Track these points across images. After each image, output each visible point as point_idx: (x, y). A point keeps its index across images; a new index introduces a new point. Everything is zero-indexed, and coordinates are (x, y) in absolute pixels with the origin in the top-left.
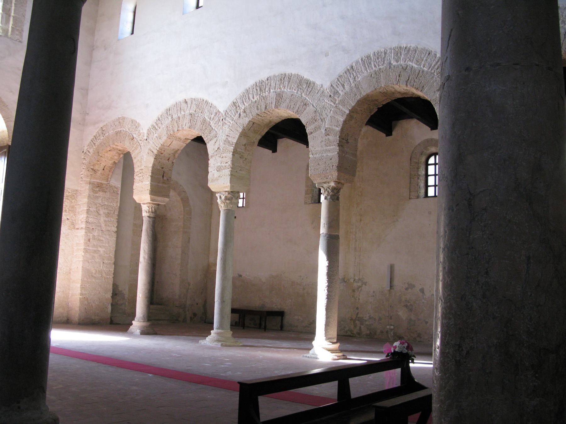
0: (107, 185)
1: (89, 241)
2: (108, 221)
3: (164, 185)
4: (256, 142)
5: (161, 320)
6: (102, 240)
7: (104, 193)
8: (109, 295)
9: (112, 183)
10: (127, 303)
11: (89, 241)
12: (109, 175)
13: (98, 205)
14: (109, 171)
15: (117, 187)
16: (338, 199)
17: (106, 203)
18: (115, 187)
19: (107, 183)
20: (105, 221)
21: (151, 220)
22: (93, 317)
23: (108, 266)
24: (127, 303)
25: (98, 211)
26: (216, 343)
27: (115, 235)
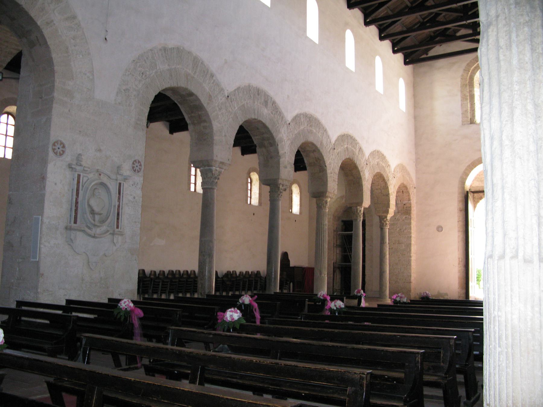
21: (385, 242)
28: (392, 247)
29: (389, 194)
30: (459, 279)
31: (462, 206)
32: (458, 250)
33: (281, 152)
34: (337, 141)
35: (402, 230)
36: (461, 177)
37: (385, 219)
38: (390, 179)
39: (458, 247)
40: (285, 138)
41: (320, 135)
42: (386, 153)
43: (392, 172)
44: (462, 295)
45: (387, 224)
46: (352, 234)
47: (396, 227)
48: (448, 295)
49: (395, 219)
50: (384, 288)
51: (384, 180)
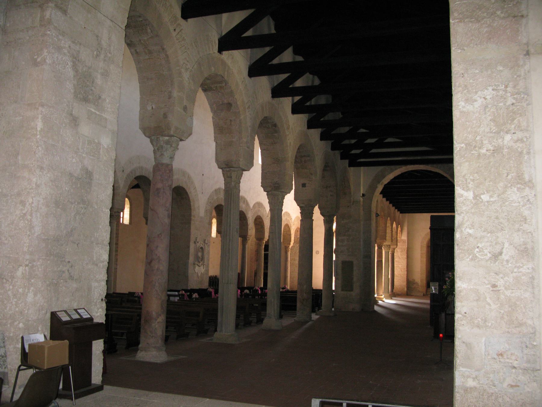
8: (405, 284)
10: (420, 287)
16: (255, 273)
17: (400, 247)
18: (404, 240)
26: (292, 144)
29: (291, 234)
33: (249, 223)
34: (185, 109)
35: (296, 253)
37: (288, 248)
38: (292, 226)
40: (250, 216)
41: (262, 211)
42: (290, 213)
43: (293, 222)
46: (268, 253)
51: (289, 227)
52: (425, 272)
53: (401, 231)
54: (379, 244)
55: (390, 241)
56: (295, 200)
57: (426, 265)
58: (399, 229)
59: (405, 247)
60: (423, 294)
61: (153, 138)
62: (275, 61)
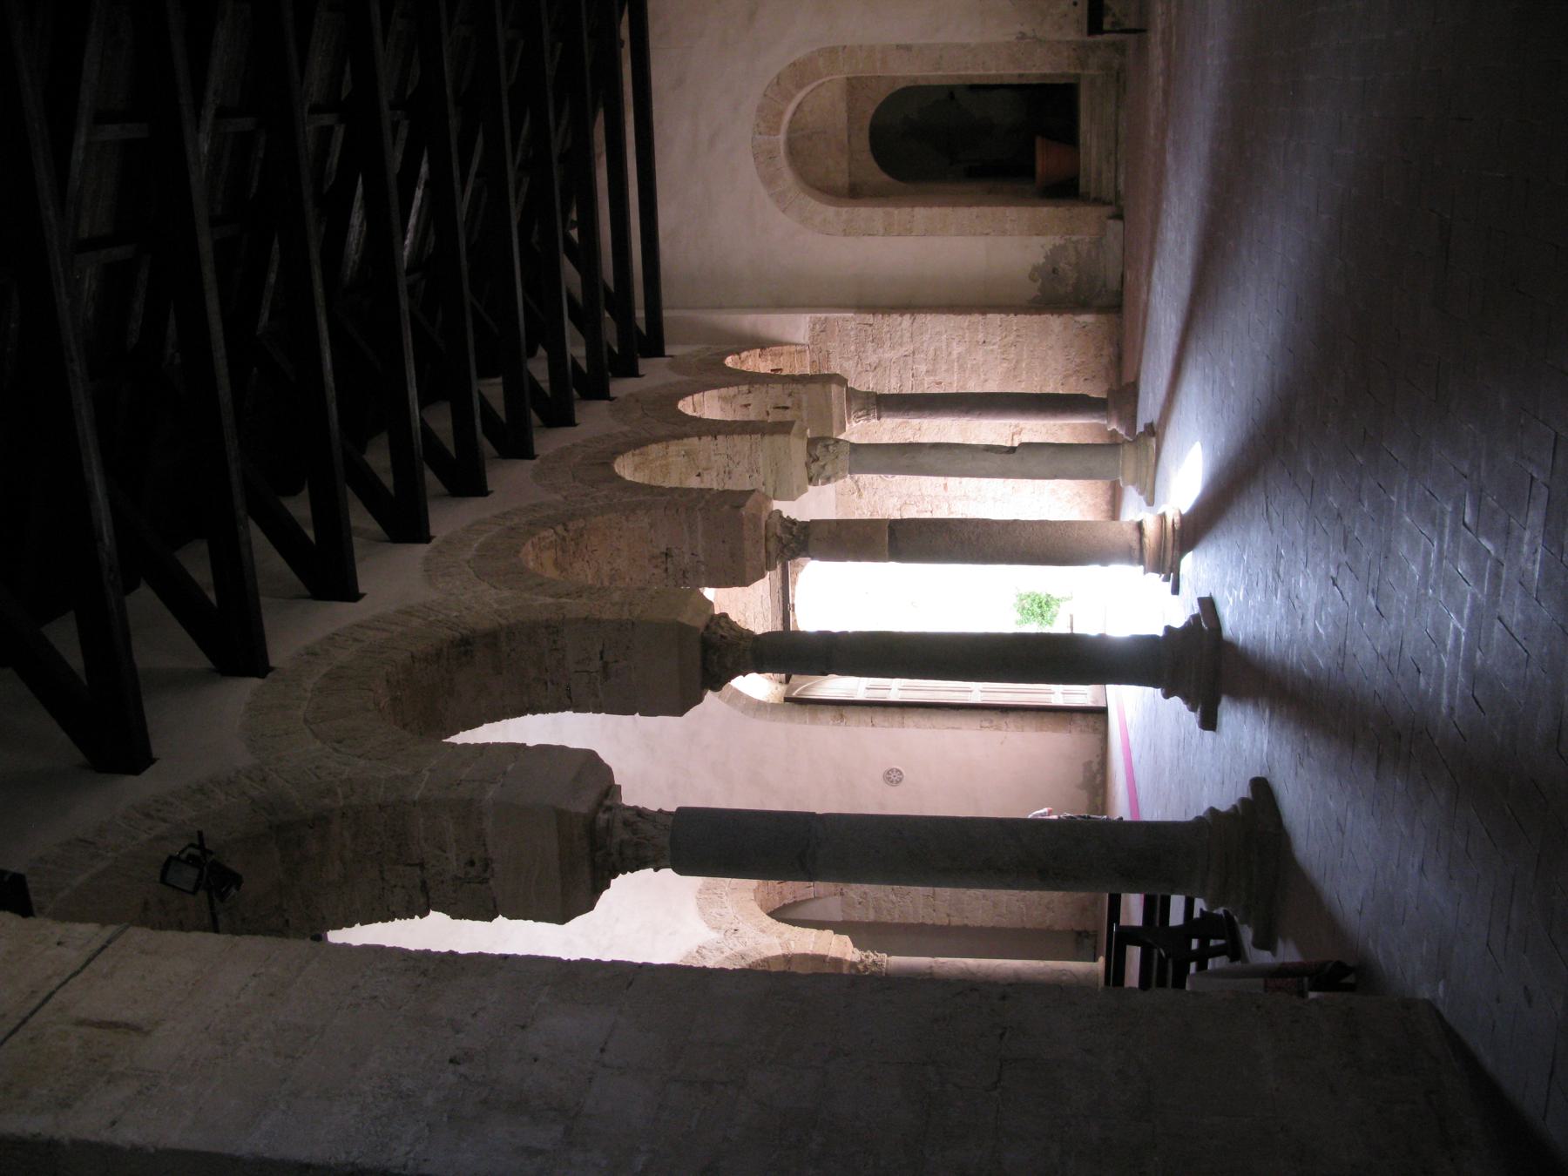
0: (813, 351)
1: (941, 383)
2: (890, 339)
3: (804, 404)
4: (686, 448)
5: (1116, 131)
6: (935, 350)
7: (830, 355)
8: (1055, 322)
9: (804, 338)
10: (1074, 238)
11: (941, 383)
12: (790, 353)
13: (860, 369)
14: (782, 354)
15: (812, 325)
17: (853, 348)
18: (813, 329)
19: (808, 352)
20: (892, 347)
21: (928, 971)
22: (1105, 360)
23: (991, 330)
24: (1074, 238)
25: (873, 368)
27: (921, 318)
28: (945, 916)
30: (1042, 730)
31: (827, 715)
32: (958, 728)
36: (742, 712)
37: (860, 967)
38: (740, 948)
39: (948, 728)
44: (1091, 723)
45: (874, 961)
47: (884, 901)
48: (1091, 762)
49: (860, 903)
50: (1064, 978)
52: (987, 210)
53: (763, 348)
54: (772, 546)
55: (779, 440)
56: (681, 714)
57: (954, 204)
58: (755, 362)
59: (849, 321)
60: (1111, 222)
61: (672, 818)
62: (388, 481)
